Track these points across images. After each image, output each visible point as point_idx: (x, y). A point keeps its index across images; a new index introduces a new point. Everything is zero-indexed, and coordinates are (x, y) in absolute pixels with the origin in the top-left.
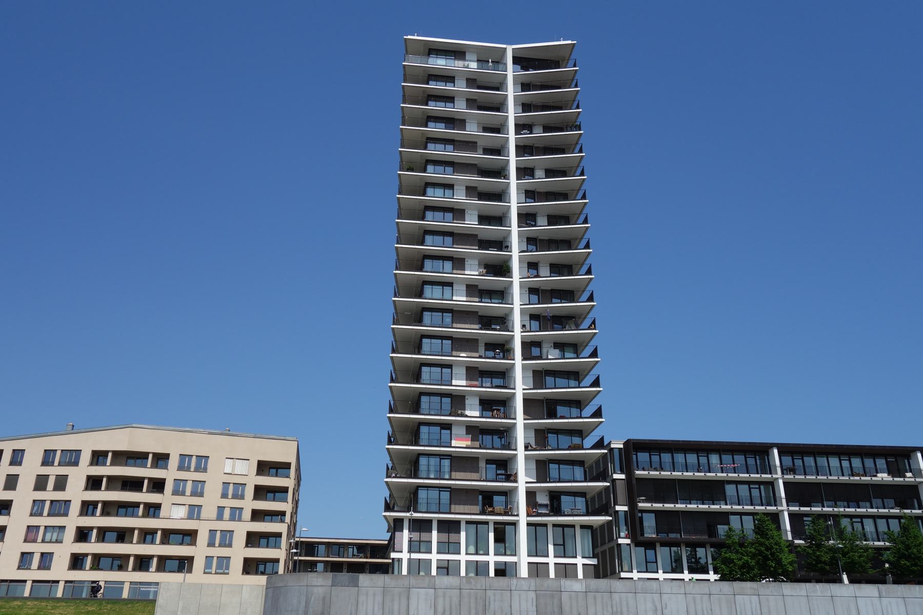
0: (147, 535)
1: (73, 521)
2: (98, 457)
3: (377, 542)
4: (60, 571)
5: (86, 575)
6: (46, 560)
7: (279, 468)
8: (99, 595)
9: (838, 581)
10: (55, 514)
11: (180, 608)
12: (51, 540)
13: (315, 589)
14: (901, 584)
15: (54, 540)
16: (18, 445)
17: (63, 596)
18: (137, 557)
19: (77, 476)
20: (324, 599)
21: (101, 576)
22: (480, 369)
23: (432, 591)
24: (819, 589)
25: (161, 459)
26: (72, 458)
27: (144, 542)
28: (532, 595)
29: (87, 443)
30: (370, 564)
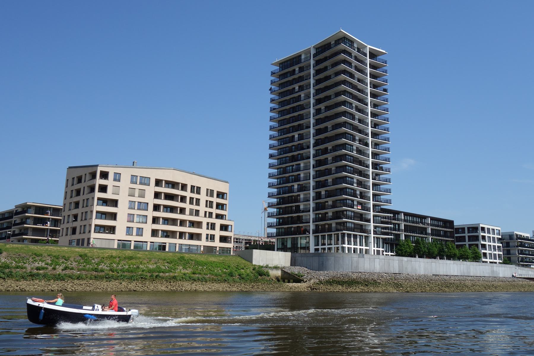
0: (182, 223)
1: (151, 213)
2: (158, 183)
3: (43, 205)
4: (147, 237)
5: (160, 240)
6: (140, 232)
7: (221, 195)
8: (167, 250)
9: (414, 256)
10: (140, 209)
11: (260, 260)
12: (140, 222)
13: (354, 258)
14: (403, 257)
15: (141, 222)
16: (118, 170)
17: (150, 249)
18: (189, 233)
19: (151, 189)
20: (357, 261)
21: (168, 241)
22: (360, 180)
23: (379, 260)
24: (433, 260)
25: (184, 187)
26: (145, 181)
27: (164, 224)
28: (398, 261)
29: (154, 174)
30: (34, 218)
